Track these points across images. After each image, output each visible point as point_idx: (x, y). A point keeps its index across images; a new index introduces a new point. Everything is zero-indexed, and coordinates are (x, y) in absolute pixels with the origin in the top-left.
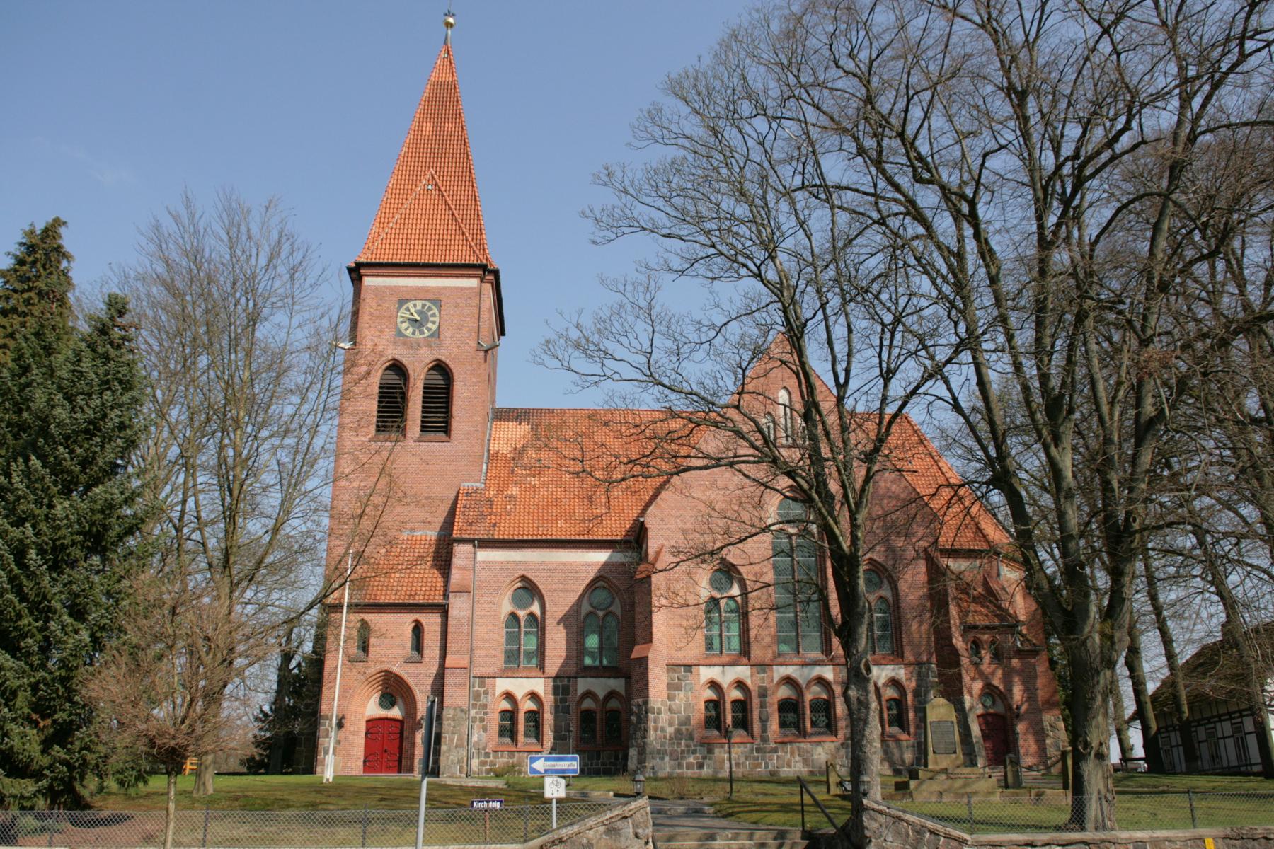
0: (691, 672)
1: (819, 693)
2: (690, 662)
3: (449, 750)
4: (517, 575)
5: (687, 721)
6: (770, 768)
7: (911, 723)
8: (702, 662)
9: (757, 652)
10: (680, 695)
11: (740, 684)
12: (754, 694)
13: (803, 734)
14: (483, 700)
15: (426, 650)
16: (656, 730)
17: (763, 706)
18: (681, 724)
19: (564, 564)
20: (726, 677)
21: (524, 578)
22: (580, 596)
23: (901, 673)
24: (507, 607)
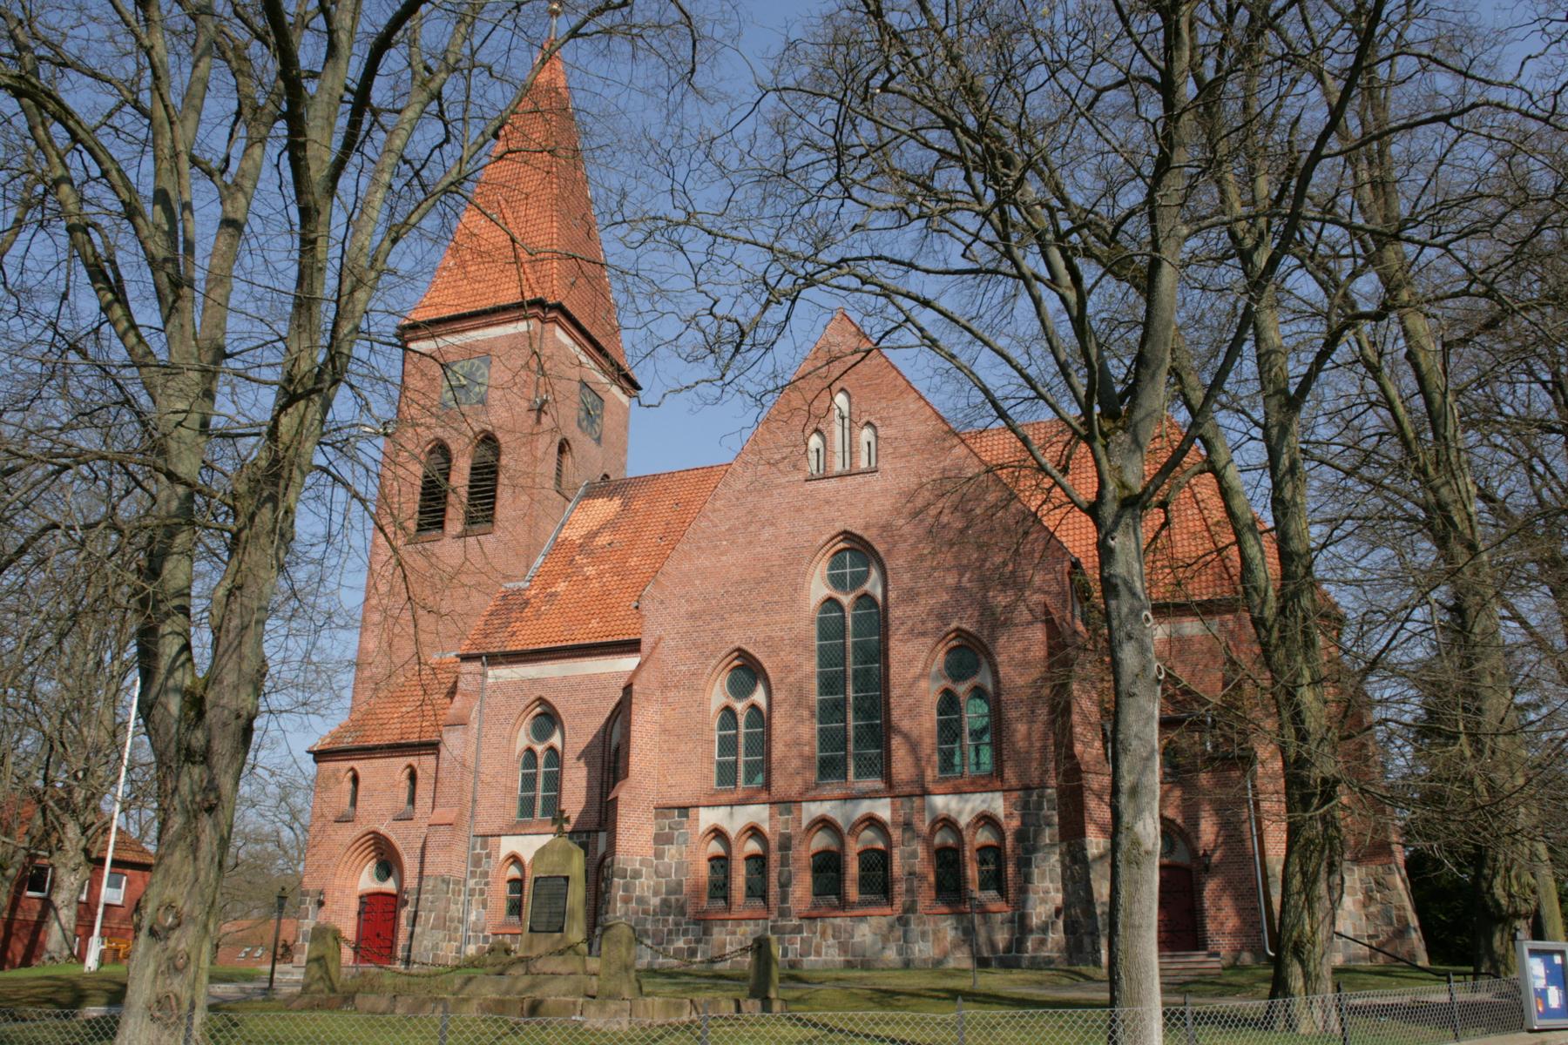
0: (687, 816)
1: (871, 841)
2: (687, 802)
3: (423, 933)
4: (532, 698)
5: (676, 889)
6: (791, 956)
7: (1010, 884)
8: (703, 801)
9: (780, 784)
10: (671, 851)
11: (754, 831)
12: (774, 843)
13: (844, 904)
14: (484, 867)
15: (418, 803)
16: (626, 901)
17: (784, 862)
18: (669, 893)
19: (590, 677)
20: (734, 820)
21: (542, 701)
22: (609, 719)
23: (997, 804)
24: (523, 740)
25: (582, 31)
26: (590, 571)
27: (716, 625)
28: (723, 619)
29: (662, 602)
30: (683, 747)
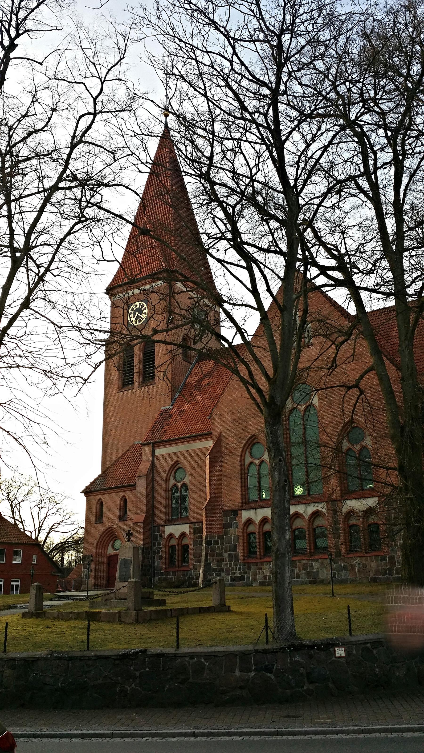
25: (209, 54)
26: (199, 398)
27: (244, 425)
28: (247, 422)
29: (220, 415)
30: (233, 482)
